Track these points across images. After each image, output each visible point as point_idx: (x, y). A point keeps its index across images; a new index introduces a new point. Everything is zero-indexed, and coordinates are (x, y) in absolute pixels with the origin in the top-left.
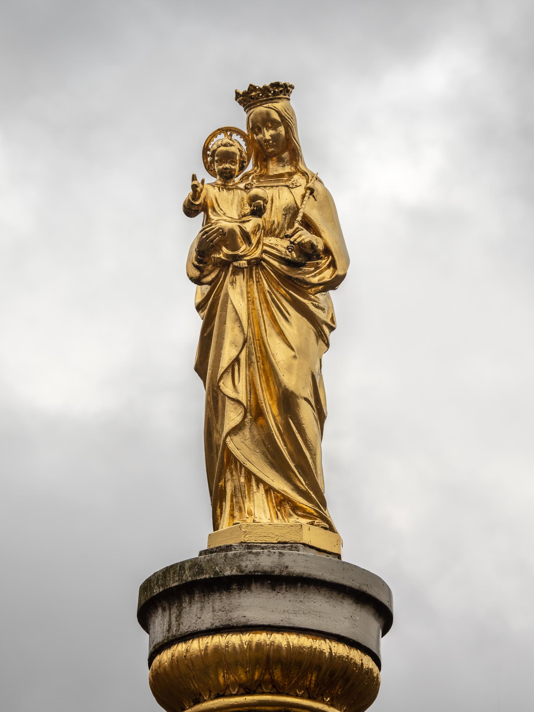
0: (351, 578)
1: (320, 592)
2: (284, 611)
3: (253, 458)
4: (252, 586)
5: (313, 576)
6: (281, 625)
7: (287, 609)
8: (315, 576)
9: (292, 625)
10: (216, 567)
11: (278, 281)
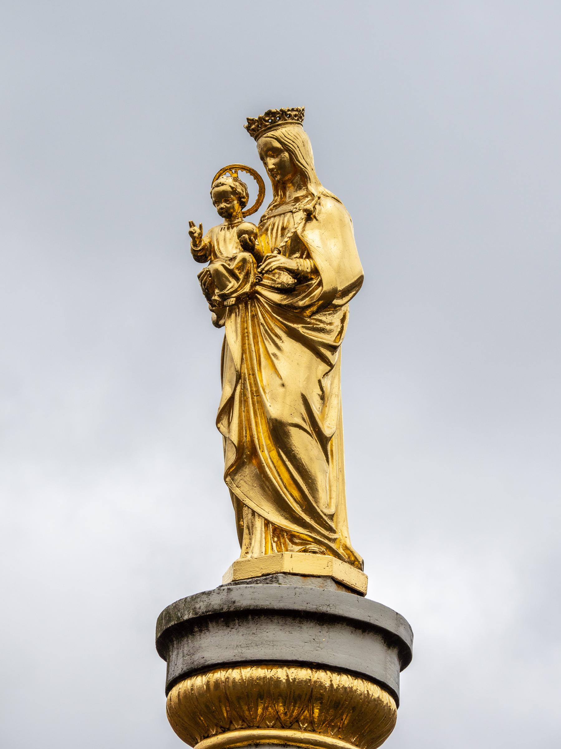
0: (305, 602)
1: (273, 621)
2: (237, 646)
3: (251, 494)
4: (210, 626)
5: (260, 606)
6: (234, 660)
7: (240, 644)
8: (263, 607)
9: (244, 659)
10: (179, 613)
11: (270, 311)
